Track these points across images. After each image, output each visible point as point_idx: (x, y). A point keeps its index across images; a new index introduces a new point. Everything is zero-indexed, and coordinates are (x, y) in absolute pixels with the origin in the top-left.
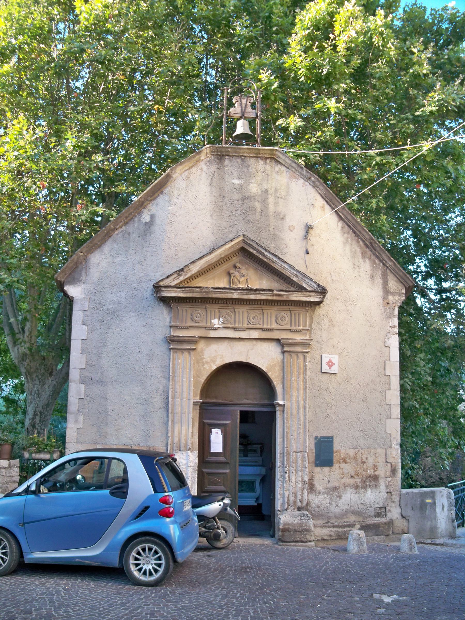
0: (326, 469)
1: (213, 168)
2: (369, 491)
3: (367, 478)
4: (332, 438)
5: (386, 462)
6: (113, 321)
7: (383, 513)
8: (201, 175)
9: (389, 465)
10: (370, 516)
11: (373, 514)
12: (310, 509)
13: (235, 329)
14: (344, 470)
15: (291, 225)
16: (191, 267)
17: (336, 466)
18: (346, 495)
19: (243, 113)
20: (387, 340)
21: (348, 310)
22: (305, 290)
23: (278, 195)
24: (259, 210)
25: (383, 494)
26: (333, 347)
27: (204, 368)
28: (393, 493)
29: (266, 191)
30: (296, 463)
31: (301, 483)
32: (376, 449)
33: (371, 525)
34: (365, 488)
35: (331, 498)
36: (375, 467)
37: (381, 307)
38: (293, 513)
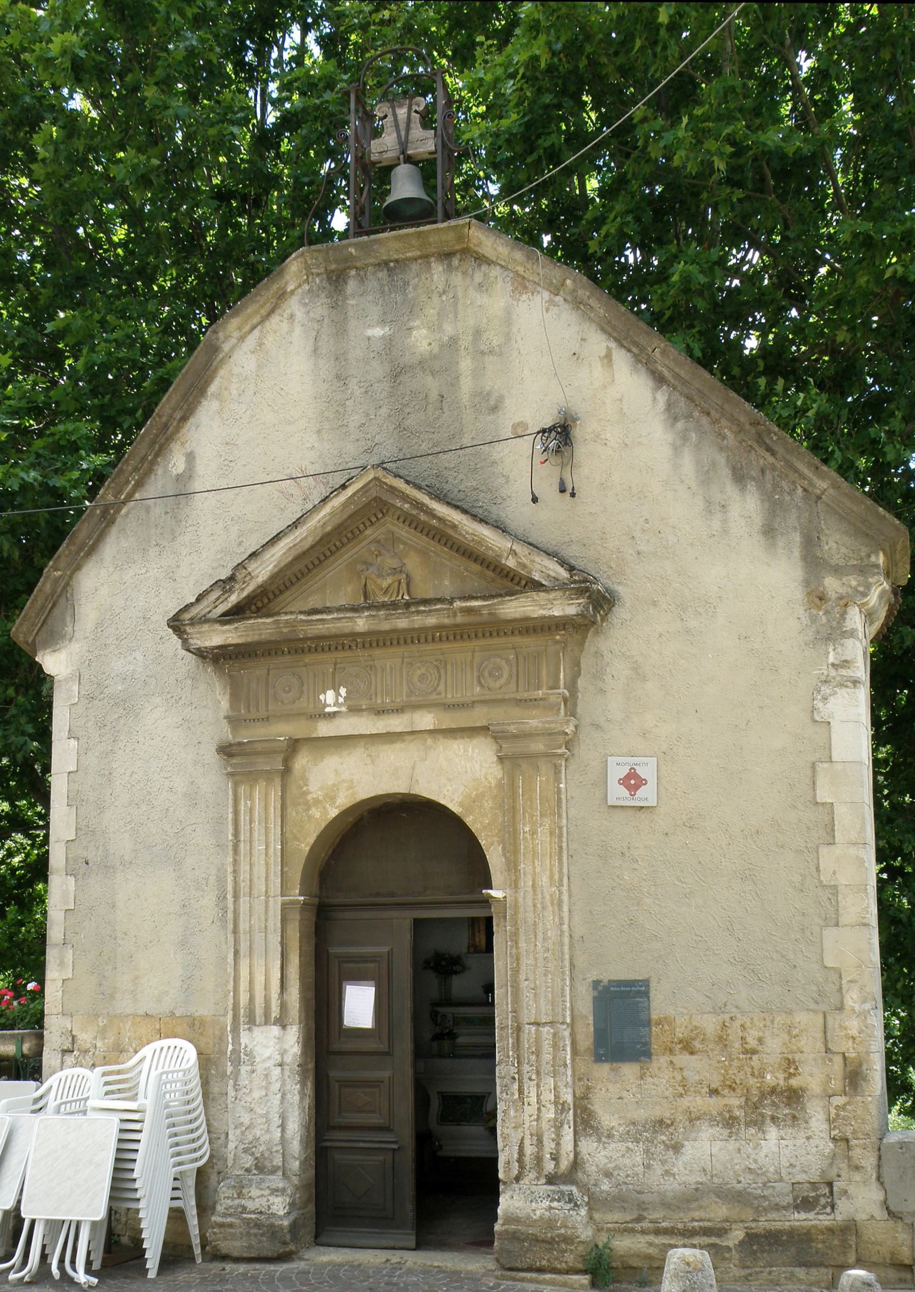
0: (629, 1070)
1: (320, 308)
2: (773, 1133)
3: (763, 1096)
4: (646, 983)
5: (827, 1050)
6: (122, 721)
7: (823, 1201)
8: (290, 332)
9: (838, 1060)
10: (777, 1207)
11: (789, 1199)
12: (585, 1179)
13: (380, 712)
14: (686, 1073)
15: (517, 420)
16: (252, 566)
17: (660, 1061)
18: (697, 1144)
19: (403, 145)
20: (819, 704)
21: (688, 631)
22: (537, 586)
23: (482, 347)
24: (434, 396)
25: (822, 1144)
26: (644, 734)
27: (310, 817)
28: (853, 1142)
29: (453, 342)
30: (538, 1054)
31: (552, 1107)
32: (790, 1012)
33: (780, 1232)
34: (758, 1123)
35: (647, 1151)
36: (790, 1065)
37: (800, 611)
38: (534, 1188)
